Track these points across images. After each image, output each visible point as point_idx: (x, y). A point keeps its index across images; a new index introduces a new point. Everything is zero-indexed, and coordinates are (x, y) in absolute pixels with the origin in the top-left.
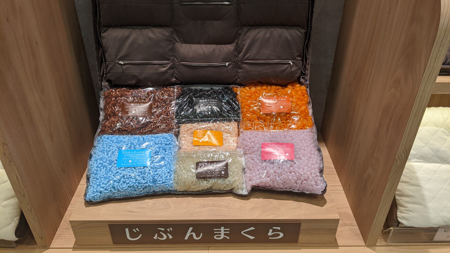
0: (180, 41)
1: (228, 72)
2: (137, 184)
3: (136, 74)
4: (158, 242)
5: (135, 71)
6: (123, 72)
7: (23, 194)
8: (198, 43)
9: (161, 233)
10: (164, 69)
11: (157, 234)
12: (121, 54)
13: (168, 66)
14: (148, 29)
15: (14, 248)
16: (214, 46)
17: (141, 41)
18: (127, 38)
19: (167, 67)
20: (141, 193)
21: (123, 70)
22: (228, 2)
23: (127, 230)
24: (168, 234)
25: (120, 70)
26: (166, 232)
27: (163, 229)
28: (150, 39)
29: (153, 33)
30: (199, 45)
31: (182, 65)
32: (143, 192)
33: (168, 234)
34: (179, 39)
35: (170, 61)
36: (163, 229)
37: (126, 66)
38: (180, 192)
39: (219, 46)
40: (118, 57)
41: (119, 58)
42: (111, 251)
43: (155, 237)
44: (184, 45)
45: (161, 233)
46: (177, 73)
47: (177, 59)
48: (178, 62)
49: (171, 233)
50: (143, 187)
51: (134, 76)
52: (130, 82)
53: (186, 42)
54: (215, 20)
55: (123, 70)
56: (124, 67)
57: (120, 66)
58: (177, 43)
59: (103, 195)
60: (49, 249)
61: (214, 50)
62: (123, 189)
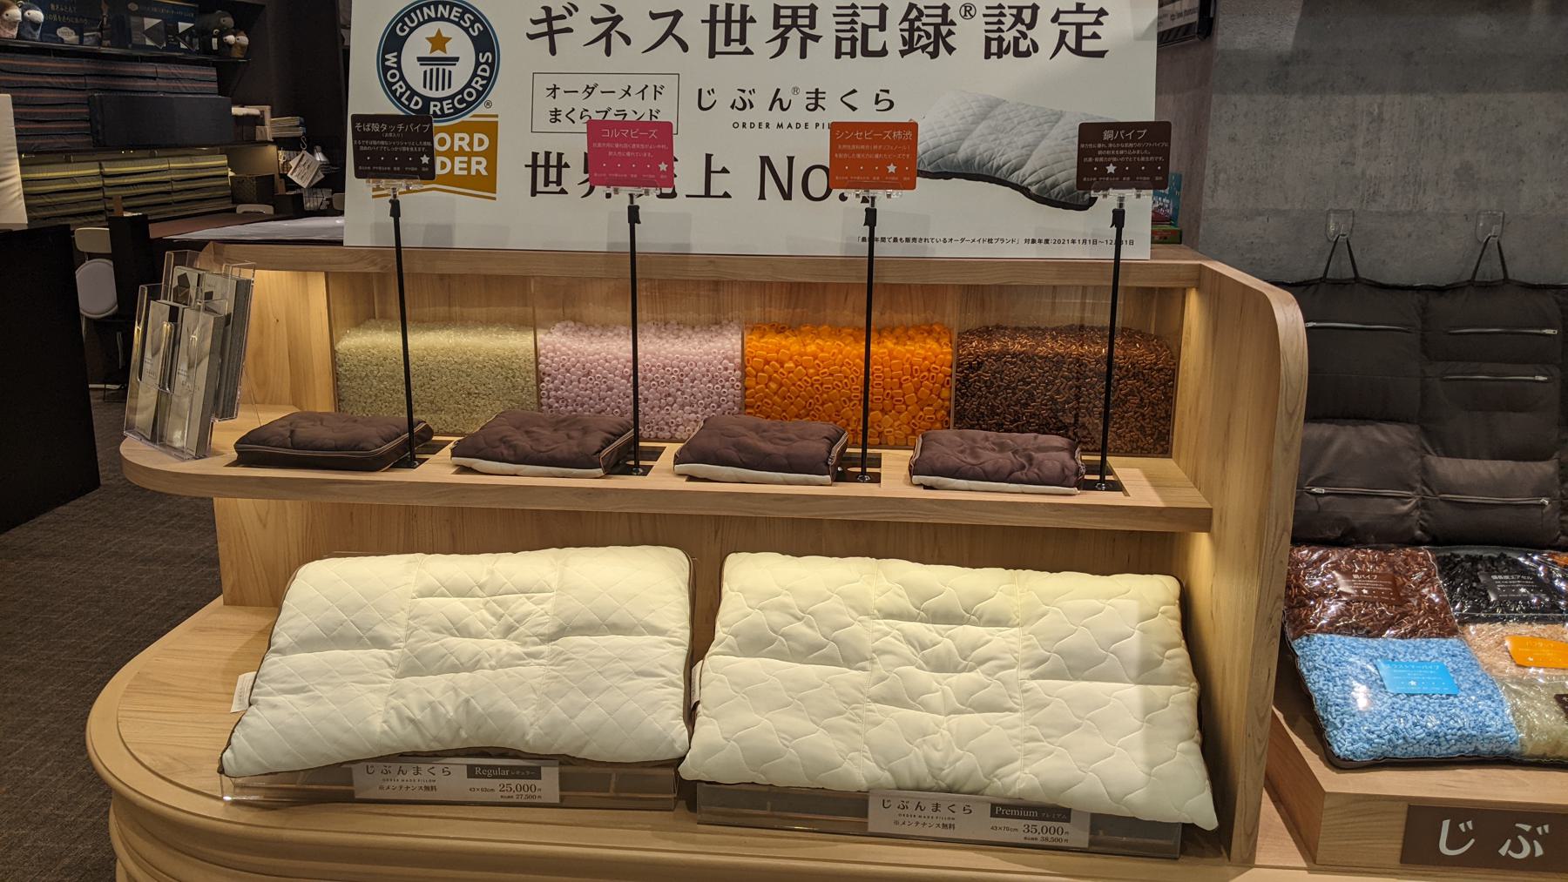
0: (1436, 452)
1: (1545, 519)
2: (1445, 729)
3: (1349, 516)
4: (1509, 864)
5: (1347, 509)
6: (1319, 512)
7: (1262, 715)
8: (1475, 457)
9: (1520, 837)
10: (1405, 508)
11: (1509, 841)
12: (1318, 473)
13: (1410, 502)
14: (1372, 424)
15: (1176, 859)
16: (1510, 464)
17: (1358, 448)
18: (1330, 441)
19: (1412, 504)
20: (1449, 751)
21: (1319, 506)
22: (1544, 375)
23: (1446, 824)
24: (1535, 842)
25: (1313, 507)
26: (1531, 837)
27: (1527, 828)
28: (1379, 444)
29: (1384, 432)
30: (1477, 462)
31: (1442, 500)
32: (1455, 750)
33: (1535, 842)
34: (1433, 448)
35: (1415, 492)
36: (1527, 828)
37: (1327, 498)
38: (1533, 757)
39: (1521, 463)
40: (1310, 480)
41: (1313, 481)
42: (1398, 879)
43: (1503, 851)
44: (1445, 460)
45: (1520, 837)
46: (1427, 517)
47: (1431, 490)
48: (1431, 494)
49: (1544, 840)
50: (1456, 737)
51: (1343, 520)
52: (1328, 534)
53: (1448, 454)
54: (1515, 411)
55: (1319, 506)
56: (1322, 500)
57: (1313, 498)
58: (1429, 456)
59: (1374, 750)
60: (1254, 869)
61: (1512, 471)
62: (1414, 739)
